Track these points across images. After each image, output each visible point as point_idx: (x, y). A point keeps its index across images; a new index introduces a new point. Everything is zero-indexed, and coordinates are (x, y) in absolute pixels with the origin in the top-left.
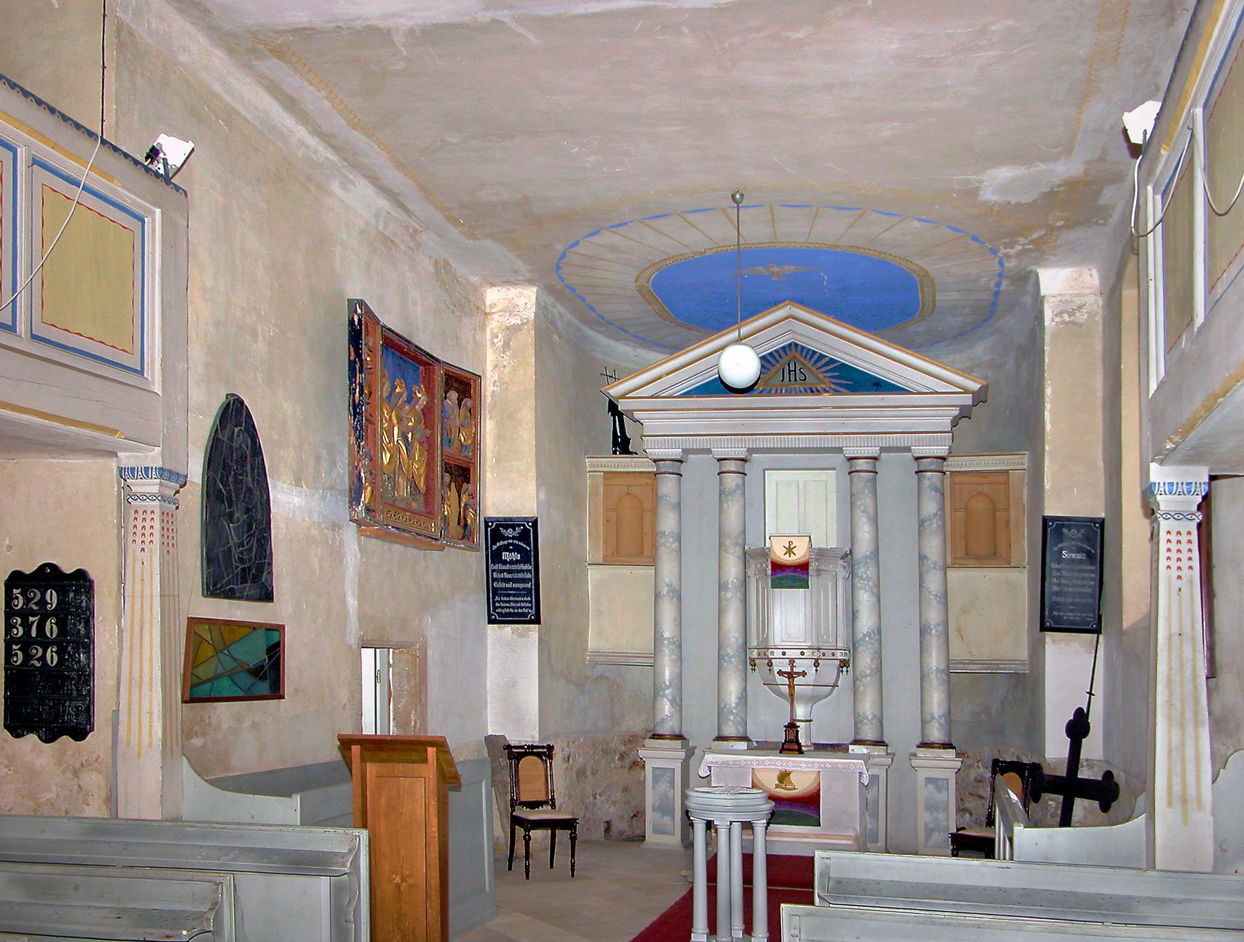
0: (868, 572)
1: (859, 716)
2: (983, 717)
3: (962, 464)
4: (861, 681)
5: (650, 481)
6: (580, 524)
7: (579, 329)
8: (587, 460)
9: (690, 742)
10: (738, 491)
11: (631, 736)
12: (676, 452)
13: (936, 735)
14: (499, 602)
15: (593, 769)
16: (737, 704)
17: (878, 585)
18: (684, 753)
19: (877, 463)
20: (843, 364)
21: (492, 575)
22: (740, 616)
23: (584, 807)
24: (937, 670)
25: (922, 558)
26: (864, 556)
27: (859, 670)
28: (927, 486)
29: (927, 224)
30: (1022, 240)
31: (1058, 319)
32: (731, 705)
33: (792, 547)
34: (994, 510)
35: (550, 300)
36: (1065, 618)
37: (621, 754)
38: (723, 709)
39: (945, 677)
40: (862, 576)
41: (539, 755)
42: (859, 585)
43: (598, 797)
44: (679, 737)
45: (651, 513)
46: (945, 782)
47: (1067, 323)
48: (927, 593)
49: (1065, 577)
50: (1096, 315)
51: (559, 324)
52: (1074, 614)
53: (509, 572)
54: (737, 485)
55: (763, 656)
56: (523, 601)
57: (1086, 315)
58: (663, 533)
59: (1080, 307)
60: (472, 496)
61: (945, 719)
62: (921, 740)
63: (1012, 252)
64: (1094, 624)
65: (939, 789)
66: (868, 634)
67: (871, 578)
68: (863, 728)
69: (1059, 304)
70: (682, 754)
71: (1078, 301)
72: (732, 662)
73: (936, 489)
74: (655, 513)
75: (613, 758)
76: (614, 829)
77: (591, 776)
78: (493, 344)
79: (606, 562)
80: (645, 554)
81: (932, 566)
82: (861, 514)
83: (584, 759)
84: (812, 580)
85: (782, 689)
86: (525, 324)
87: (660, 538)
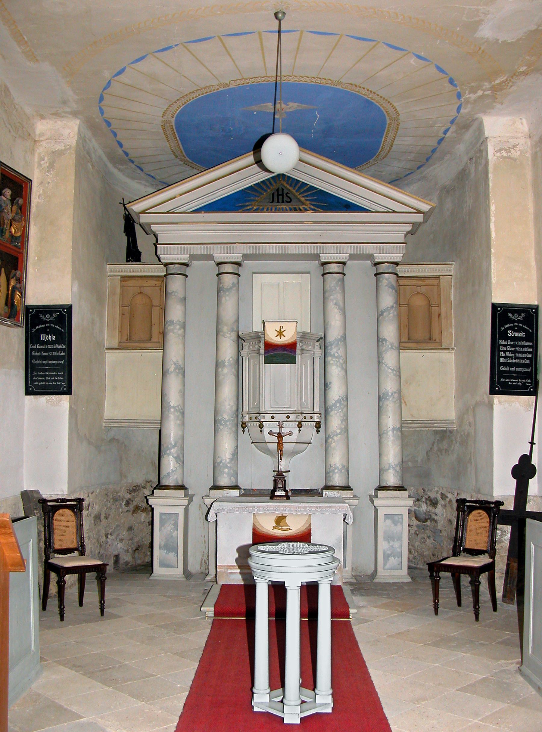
0: (339, 352)
1: (331, 467)
2: (410, 464)
3: (405, 271)
4: (332, 438)
5: (158, 283)
6: (101, 317)
7: (106, 165)
8: (108, 266)
9: (190, 491)
10: (234, 289)
11: (135, 486)
12: (184, 257)
13: (392, 479)
14: (36, 376)
15: (106, 514)
16: (231, 460)
17: (346, 362)
18: (187, 501)
19: (344, 267)
20: (321, 190)
21: (31, 353)
22: (234, 388)
23: (99, 546)
24: (393, 429)
25: (380, 340)
26: (335, 339)
27: (330, 430)
28: (385, 284)
29: (421, 62)
30: (487, 85)
31: (498, 155)
32: (226, 460)
33: (282, 330)
34: (430, 305)
35: (88, 134)
36: (510, 383)
37: (127, 501)
38: (219, 464)
39: (399, 434)
40: (334, 355)
41: (70, 507)
42: (332, 362)
43: (109, 537)
44: (181, 487)
45: (159, 308)
46: (400, 517)
47: (505, 158)
48: (386, 368)
49: (510, 351)
50: (526, 152)
51: (93, 156)
52: (517, 380)
53: (45, 350)
54: (233, 283)
55: (254, 420)
56: (57, 376)
57: (519, 153)
58: (172, 322)
59: (514, 147)
60: (19, 280)
61: (400, 466)
62: (379, 485)
63: (473, 97)
64: (531, 388)
65: (395, 523)
66: (339, 401)
67: (341, 356)
68: (334, 476)
69: (498, 144)
70: (185, 502)
71: (513, 142)
72: (227, 425)
73: (392, 287)
74: (164, 309)
75: (121, 504)
76: (121, 561)
77: (104, 520)
78: (40, 165)
79: (120, 347)
80: (153, 340)
81: (390, 346)
82: (333, 306)
83: (99, 506)
84: (298, 358)
85: (269, 447)
86: (67, 149)
87: (169, 325)
